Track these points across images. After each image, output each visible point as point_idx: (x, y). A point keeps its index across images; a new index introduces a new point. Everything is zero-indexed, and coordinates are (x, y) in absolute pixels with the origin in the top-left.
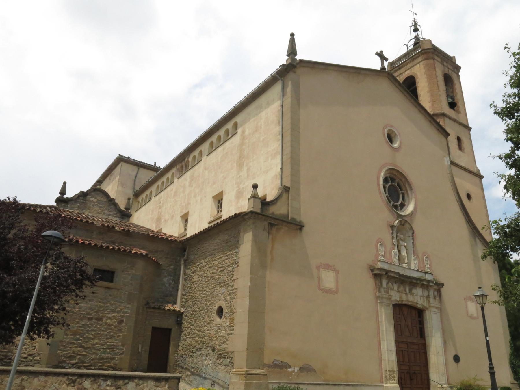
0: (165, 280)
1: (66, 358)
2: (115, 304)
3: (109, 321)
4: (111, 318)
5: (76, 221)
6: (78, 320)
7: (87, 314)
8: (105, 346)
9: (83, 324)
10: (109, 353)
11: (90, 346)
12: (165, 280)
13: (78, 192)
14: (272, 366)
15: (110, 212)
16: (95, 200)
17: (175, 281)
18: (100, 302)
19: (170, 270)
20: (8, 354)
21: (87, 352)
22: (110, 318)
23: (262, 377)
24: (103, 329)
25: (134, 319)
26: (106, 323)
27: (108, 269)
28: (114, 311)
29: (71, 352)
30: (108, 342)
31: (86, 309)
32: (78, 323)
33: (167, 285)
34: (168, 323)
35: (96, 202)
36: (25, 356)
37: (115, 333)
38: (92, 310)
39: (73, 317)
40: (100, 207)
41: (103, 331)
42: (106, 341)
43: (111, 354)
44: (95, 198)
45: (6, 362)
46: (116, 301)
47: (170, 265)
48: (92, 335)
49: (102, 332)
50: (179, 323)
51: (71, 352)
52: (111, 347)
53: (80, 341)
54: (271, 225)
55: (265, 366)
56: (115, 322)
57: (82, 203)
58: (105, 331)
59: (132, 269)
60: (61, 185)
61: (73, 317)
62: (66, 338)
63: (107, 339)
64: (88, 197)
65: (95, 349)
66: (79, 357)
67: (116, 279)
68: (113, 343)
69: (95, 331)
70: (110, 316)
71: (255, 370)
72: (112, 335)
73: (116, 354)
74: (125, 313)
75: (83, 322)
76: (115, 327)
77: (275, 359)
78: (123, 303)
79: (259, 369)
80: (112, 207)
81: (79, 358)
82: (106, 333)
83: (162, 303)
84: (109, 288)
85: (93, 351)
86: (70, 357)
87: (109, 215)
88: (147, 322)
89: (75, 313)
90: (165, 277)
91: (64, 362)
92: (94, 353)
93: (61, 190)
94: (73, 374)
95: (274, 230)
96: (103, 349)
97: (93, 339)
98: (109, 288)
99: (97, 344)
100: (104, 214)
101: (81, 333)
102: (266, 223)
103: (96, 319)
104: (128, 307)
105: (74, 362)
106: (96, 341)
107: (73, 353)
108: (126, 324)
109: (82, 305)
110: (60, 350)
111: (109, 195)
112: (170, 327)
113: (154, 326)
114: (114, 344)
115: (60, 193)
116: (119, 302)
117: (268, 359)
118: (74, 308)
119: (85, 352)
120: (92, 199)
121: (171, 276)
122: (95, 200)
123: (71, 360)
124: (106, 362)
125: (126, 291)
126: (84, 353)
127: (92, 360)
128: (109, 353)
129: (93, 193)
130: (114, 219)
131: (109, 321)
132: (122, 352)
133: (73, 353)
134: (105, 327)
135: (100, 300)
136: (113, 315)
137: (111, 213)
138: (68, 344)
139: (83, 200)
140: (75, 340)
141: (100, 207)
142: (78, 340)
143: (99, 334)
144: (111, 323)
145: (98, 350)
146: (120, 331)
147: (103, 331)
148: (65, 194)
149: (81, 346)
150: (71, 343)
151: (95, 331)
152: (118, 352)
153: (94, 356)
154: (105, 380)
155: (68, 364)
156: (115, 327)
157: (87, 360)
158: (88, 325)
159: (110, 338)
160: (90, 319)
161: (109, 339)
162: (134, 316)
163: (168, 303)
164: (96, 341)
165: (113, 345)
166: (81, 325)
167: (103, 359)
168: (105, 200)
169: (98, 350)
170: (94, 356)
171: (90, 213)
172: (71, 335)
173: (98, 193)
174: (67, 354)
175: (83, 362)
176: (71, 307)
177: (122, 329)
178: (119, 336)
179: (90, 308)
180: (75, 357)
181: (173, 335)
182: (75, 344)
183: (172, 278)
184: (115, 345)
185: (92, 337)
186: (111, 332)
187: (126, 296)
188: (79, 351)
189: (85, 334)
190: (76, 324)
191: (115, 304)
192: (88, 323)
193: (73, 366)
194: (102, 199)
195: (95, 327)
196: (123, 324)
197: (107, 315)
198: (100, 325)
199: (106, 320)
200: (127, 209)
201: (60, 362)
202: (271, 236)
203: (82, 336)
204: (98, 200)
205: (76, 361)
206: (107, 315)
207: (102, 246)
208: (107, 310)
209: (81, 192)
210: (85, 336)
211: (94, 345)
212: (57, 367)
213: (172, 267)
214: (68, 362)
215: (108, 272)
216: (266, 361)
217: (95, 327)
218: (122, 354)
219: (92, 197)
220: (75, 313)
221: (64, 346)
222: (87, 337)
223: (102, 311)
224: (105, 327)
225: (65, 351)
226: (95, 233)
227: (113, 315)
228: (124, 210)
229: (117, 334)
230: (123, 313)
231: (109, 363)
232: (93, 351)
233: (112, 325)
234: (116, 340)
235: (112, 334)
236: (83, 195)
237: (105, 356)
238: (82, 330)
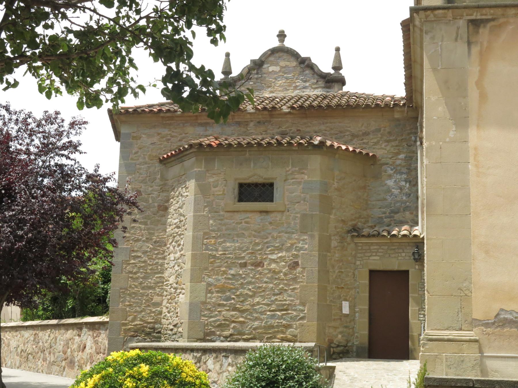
0: (390, 183)
1: (214, 327)
2: (280, 237)
3: (273, 266)
4: (276, 260)
5: (398, 109)
6: (224, 269)
7: (236, 258)
8: (274, 307)
9: (232, 275)
10: (281, 317)
11: (248, 307)
12: (390, 183)
13: (248, 63)
14: (493, 323)
15: (305, 82)
16: (276, 69)
17: (410, 182)
18: (255, 236)
19: (398, 162)
20: (156, 326)
21: (246, 318)
22: (274, 261)
23: (465, 345)
24: (265, 279)
25: (317, 259)
26: (270, 270)
27: (260, 181)
28: (280, 250)
29: (221, 318)
30: (276, 300)
31: (234, 250)
32: (225, 272)
33: (396, 192)
34: (395, 262)
35: (280, 71)
36: (171, 327)
37: (286, 285)
38: (244, 251)
39: (216, 265)
40: (287, 79)
41: (266, 282)
42: (273, 298)
43: (284, 319)
44: (277, 65)
45: (154, 337)
46: (282, 232)
47: (398, 154)
48: (250, 290)
49: (264, 285)
50: (419, 258)
51: (221, 318)
52: (284, 308)
53: (233, 301)
54: (475, 24)
55: (474, 323)
56: (284, 267)
57: (257, 79)
58: (270, 283)
59: (303, 173)
60: (224, 57)
61: (216, 265)
62: (210, 298)
63: (275, 295)
64: (265, 66)
65: (257, 313)
66: (233, 325)
67: (277, 194)
68: (285, 300)
69: (254, 283)
70: (274, 257)
71: (447, 332)
72: (282, 289)
73: (293, 319)
74: (299, 251)
75: (232, 272)
76: (285, 274)
77: (502, 310)
78: (293, 233)
79: (461, 330)
80: (307, 72)
81: (234, 328)
82: (271, 285)
83: (388, 226)
84: (267, 212)
85: (255, 315)
86: (220, 326)
87: (305, 88)
88: (358, 263)
89: (218, 258)
90: (390, 177)
91: (213, 333)
92: (256, 319)
93: (224, 68)
94: (197, 350)
95: (484, 32)
96: (270, 311)
97: (251, 297)
98: (267, 212)
99: (258, 303)
100: (296, 88)
101: (232, 289)
102: (462, 23)
103: (252, 265)
104: (303, 240)
105: (226, 333)
106: (257, 300)
107: (224, 320)
108: (304, 268)
109: (228, 244)
110: (204, 316)
111: (297, 54)
112: (404, 268)
113: (373, 268)
114: (287, 303)
115: (223, 73)
116: (286, 233)
117: (482, 308)
118: (217, 250)
119: (243, 317)
120: (271, 69)
121: (402, 173)
122: (276, 69)
123: (223, 331)
124: (278, 332)
125: (296, 213)
126: (241, 319)
127: (255, 329)
128: (281, 317)
129: (272, 59)
130: (314, 92)
131: (273, 266)
132: (302, 315)
133: (224, 320)
134: (269, 275)
135: (254, 233)
136: (280, 255)
137: (307, 84)
138: (214, 307)
139: (257, 73)
140: (224, 300)
141: (287, 79)
142: (228, 299)
143: (260, 288)
144: (278, 269)
145: (262, 313)
146: (295, 279)
147: (266, 282)
148: (231, 73)
149: (235, 309)
150: (220, 305)
151: (254, 283)
152: (297, 316)
153: (256, 324)
154: (226, 357)
155: (220, 336)
156: (285, 274)
157: (247, 330)
158: (241, 275)
159: (280, 294)
160: (244, 265)
161: (277, 294)
162: (316, 253)
163: (401, 223)
164: (257, 300)
165: (285, 305)
166: (230, 277)
167: (272, 327)
168: (294, 64)
169: (262, 313)
170: (256, 324)
171: (272, 92)
172: (218, 292)
173: (281, 54)
174: (214, 321)
175: (241, 333)
176: (212, 250)
177: (299, 276)
178: (294, 289)
179: (240, 249)
180: (228, 326)
181: (412, 281)
182: (224, 305)
183: (404, 176)
184: (288, 305)
185: (250, 293)
186: (279, 284)
187: (298, 221)
188: (232, 316)
189: (237, 289)
190: (222, 275)
191: (280, 237)
192: (241, 272)
193: (226, 338)
194: (288, 63)
195: (252, 278)
196: (299, 269)
197: (270, 256)
198: (260, 274)
199: (269, 264)
200: (337, 67)
201: (206, 334)
202: (475, 50)
203: (234, 293)
204: (282, 67)
205: (230, 332)
206: (270, 256)
207: (239, 144)
208: (268, 247)
209: (253, 62)
210: (238, 293)
211: (254, 305)
212: (204, 340)
213: (402, 156)
214: (218, 333)
215: (264, 185)
216: (476, 315)
217: (252, 278)
218: (302, 318)
219: (272, 64)
220: (218, 258)
221: (209, 309)
222: (241, 294)
223: (259, 250)
224: (269, 275)
225: (211, 317)
226: (252, 124)
227: (280, 255)
228: (332, 72)
229: (290, 285)
230: (296, 250)
231: (283, 333)
232: (255, 315)
233: (280, 272)
234: (290, 296)
235: (281, 286)
236: (257, 65)
237: (274, 322)
238: (232, 284)
